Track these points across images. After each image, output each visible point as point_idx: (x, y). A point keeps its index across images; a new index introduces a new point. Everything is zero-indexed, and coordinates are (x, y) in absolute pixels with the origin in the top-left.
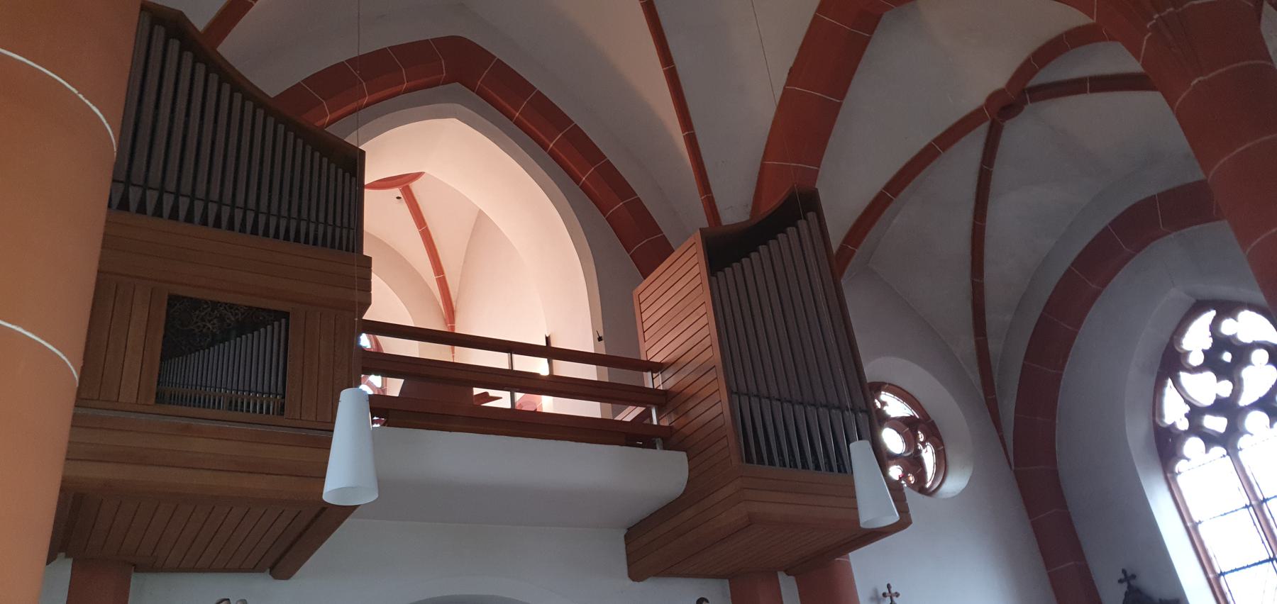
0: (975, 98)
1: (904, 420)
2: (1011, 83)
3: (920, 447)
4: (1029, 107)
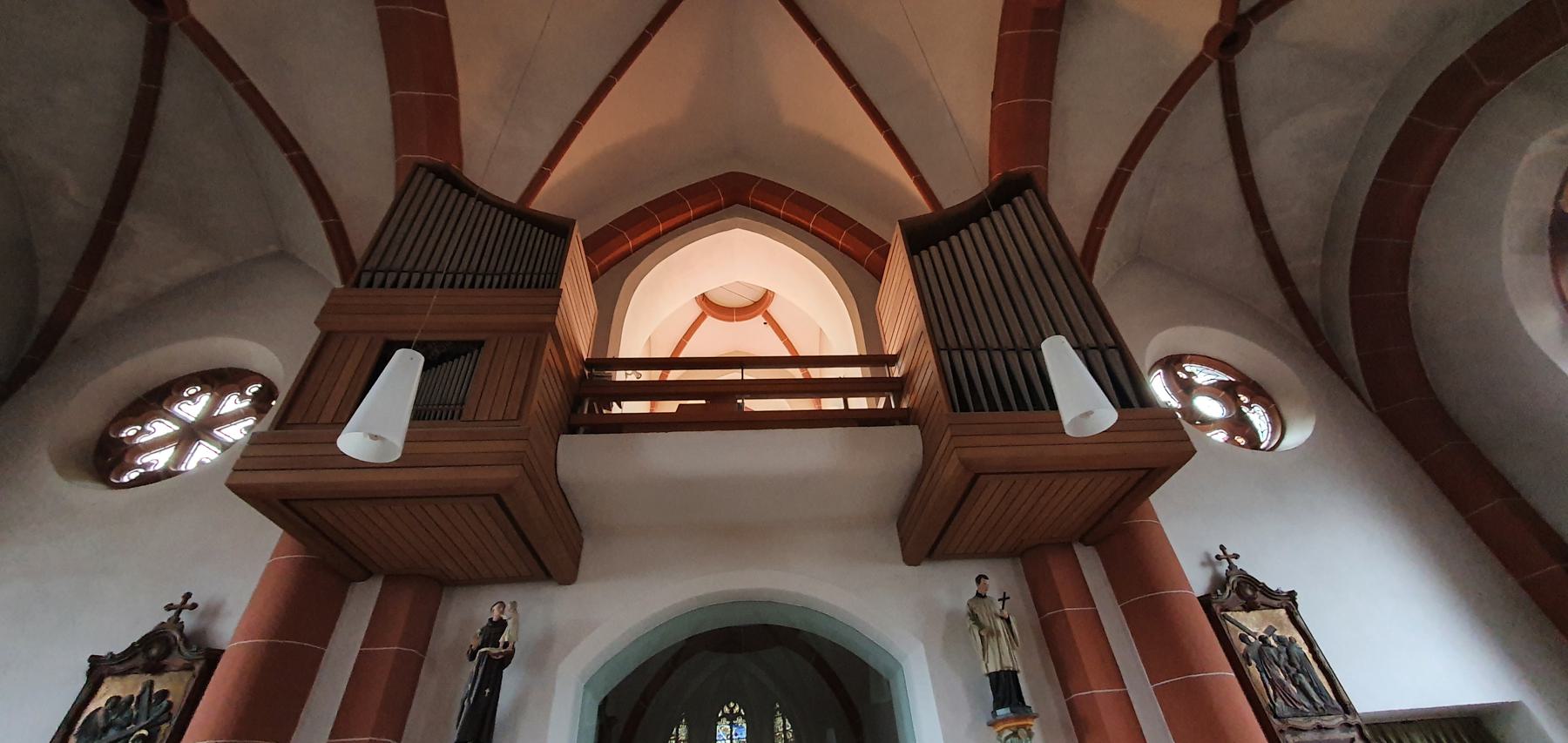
0: (1192, 46)
1: (1221, 385)
2: (1222, 16)
3: (1245, 409)
4: (1256, 31)
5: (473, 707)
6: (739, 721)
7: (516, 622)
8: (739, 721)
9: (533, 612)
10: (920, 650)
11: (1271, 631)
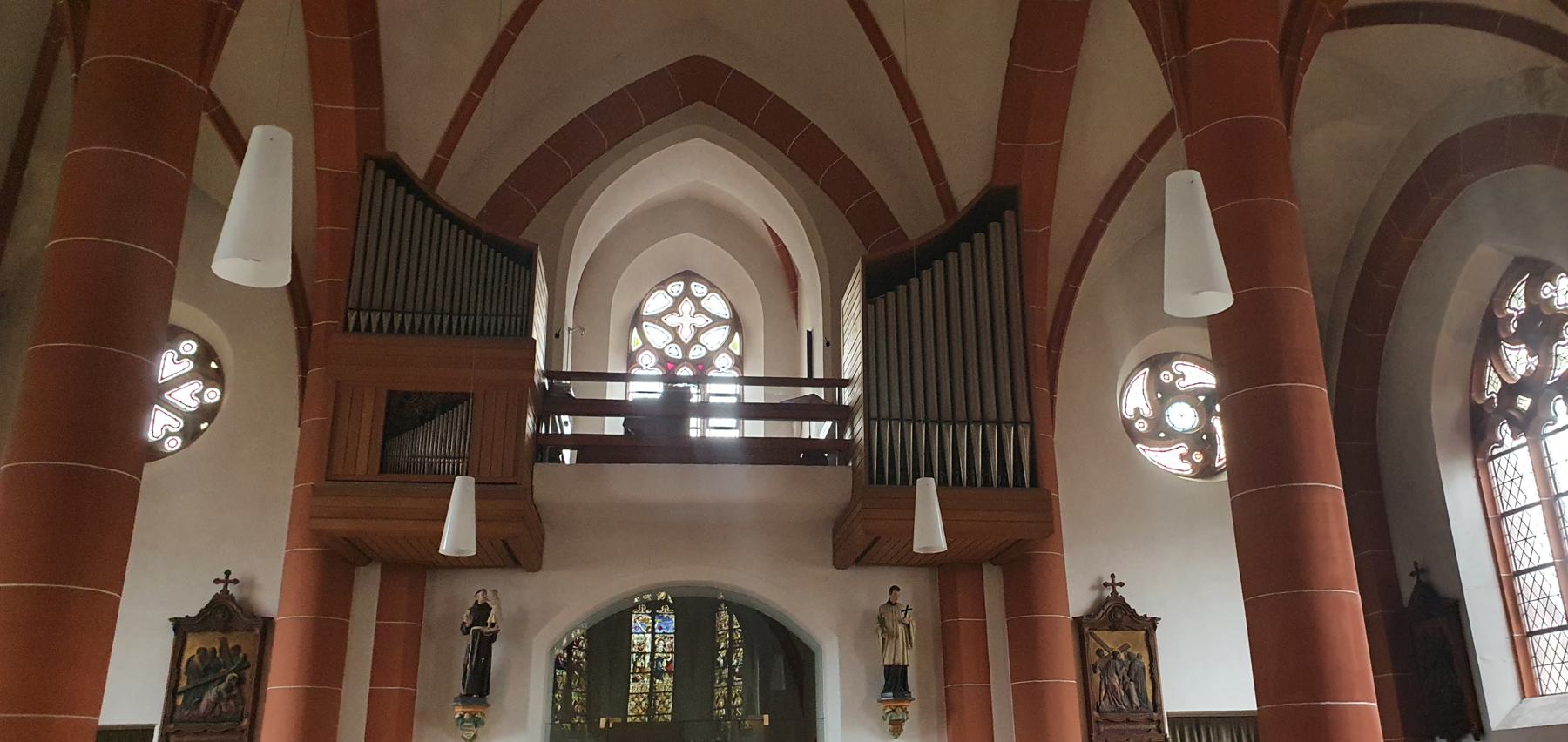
5: (474, 671)
6: (665, 610)
7: (499, 607)
8: (665, 610)
9: (510, 594)
10: (835, 640)
11: (1124, 648)
